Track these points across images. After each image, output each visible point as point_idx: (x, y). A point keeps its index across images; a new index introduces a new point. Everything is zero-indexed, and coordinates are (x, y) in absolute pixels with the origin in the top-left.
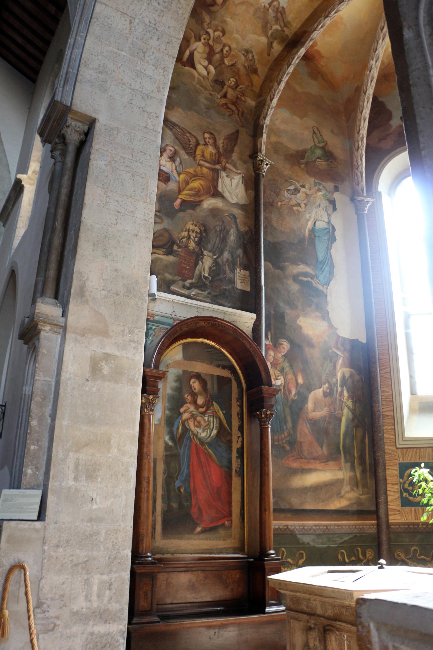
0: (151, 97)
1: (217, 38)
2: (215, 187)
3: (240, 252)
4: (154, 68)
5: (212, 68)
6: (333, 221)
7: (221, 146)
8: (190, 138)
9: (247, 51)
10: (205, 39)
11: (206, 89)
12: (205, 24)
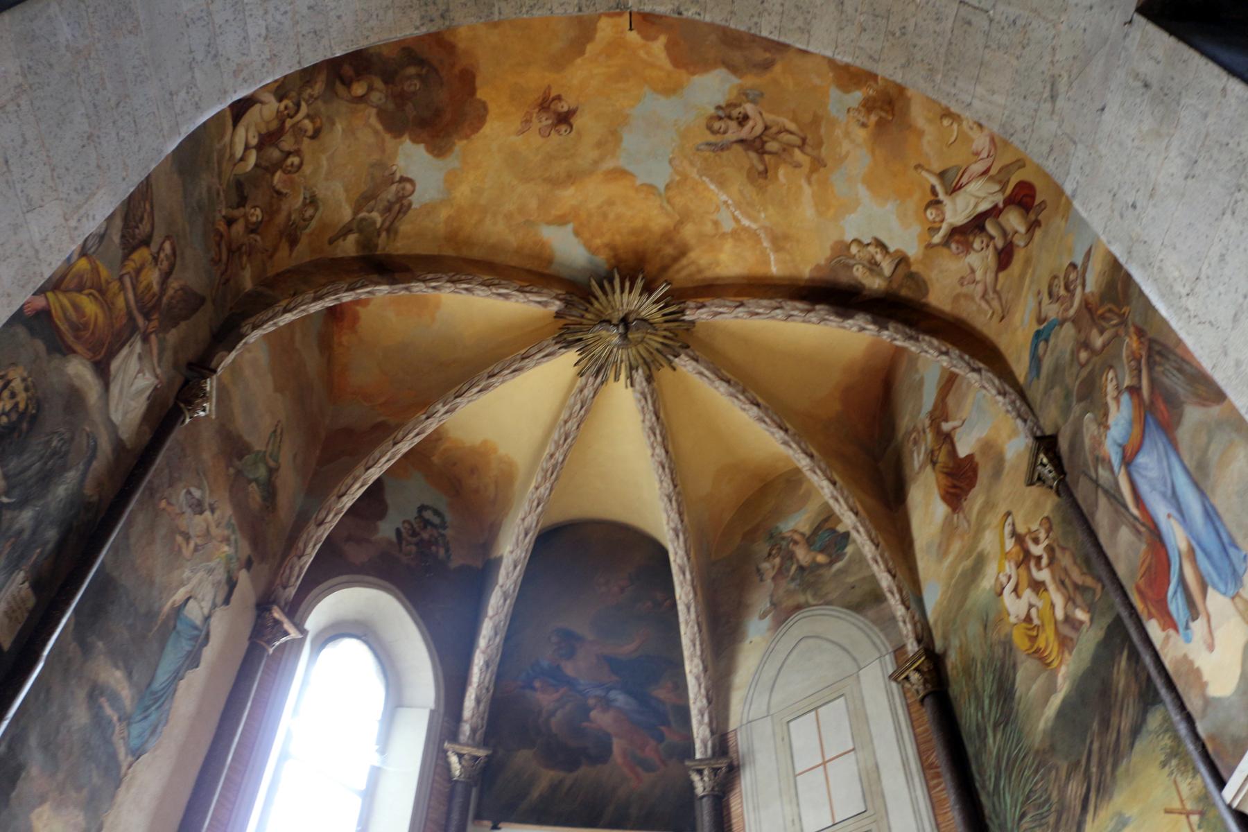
0: (218, 65)
1: (300, 129)
2: (112, 354)
3: (52, 534)
4: (264, 32)
5: (252, 158)
6: (214, 622)
7: (170, 292)
8: (146, 216)
9: (313, 201)
10: (286, 108)
11: (220, 176)
12: (309, 91)
